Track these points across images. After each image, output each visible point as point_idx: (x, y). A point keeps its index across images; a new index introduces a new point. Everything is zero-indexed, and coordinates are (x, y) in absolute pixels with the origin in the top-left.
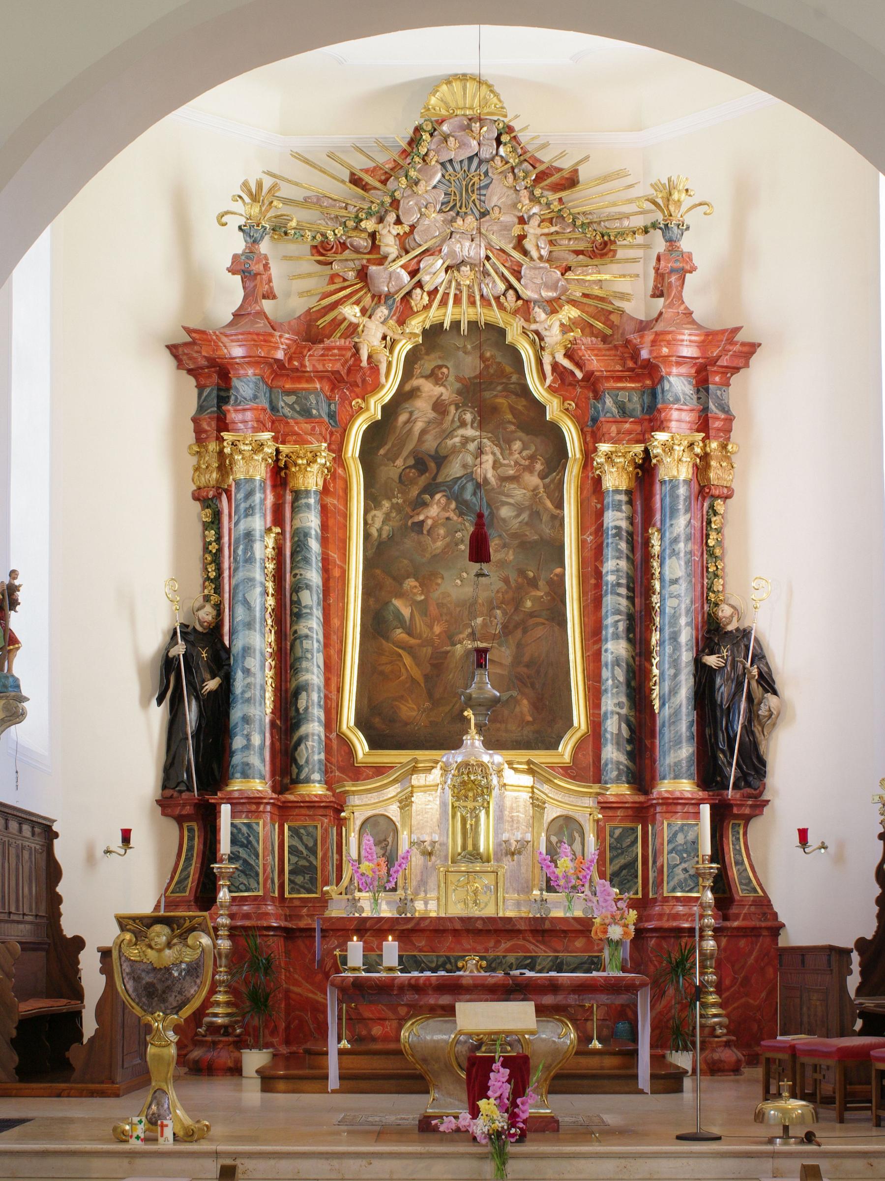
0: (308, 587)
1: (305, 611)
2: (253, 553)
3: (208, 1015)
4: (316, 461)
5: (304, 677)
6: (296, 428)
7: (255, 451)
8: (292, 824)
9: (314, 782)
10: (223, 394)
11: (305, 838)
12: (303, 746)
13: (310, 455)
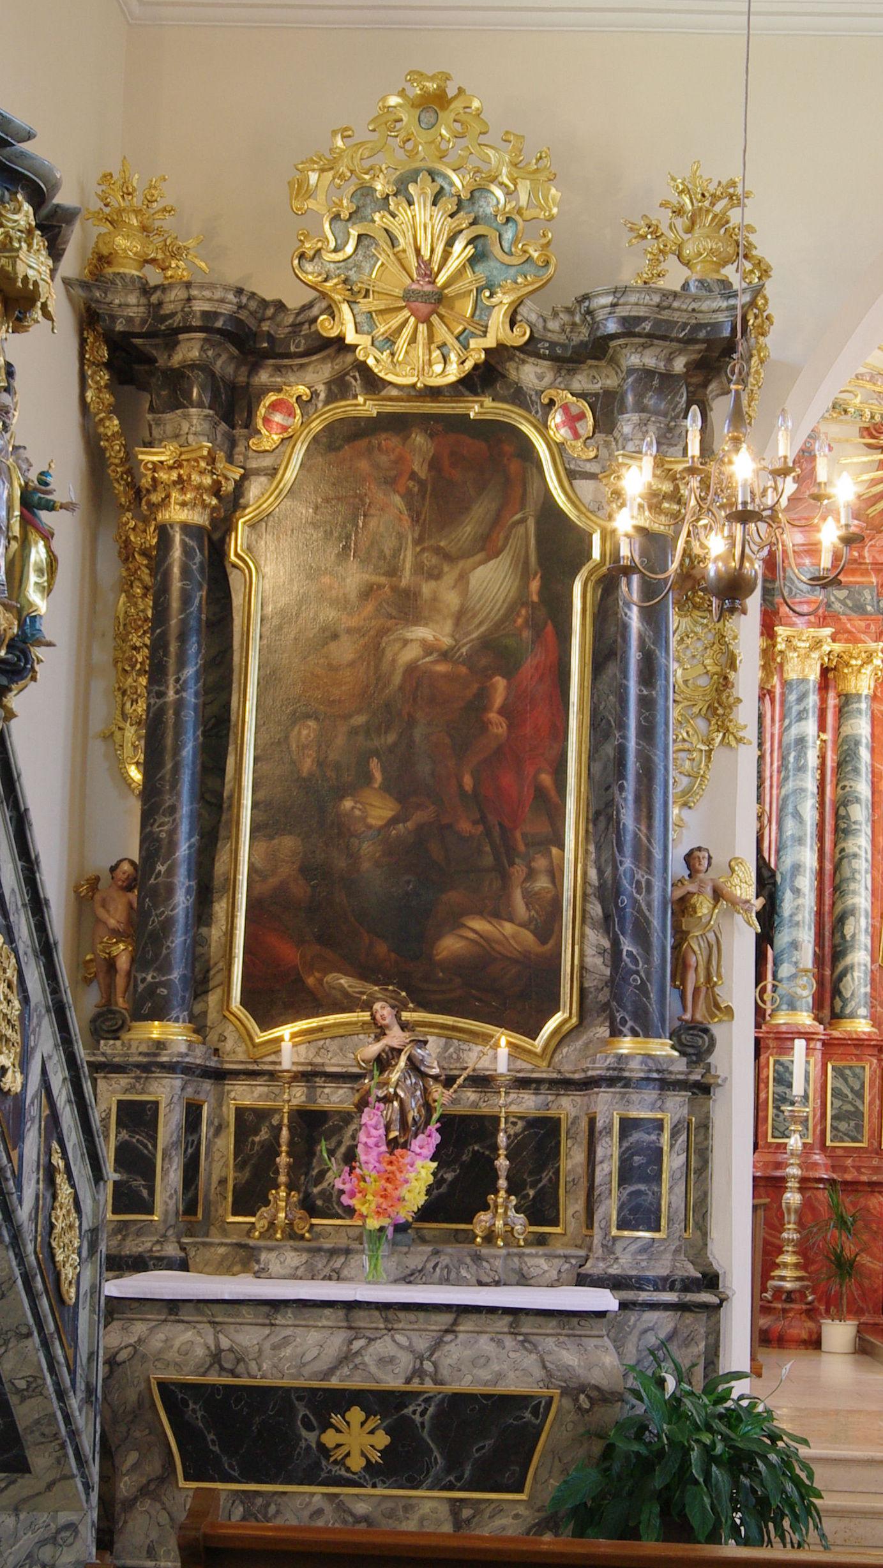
0: (858, 800)
1: (854, 827)
2: (806, 761)
3: (773, 1278)
4: (871, 661)
5: (851, 901)
6: (848, 625)
7: (812, 649)
8: (838, 1064)
9: (858, 1017)
10: (768, 585)
11: (850, 1079)
12: (849, 977)
13: (864, 655)
